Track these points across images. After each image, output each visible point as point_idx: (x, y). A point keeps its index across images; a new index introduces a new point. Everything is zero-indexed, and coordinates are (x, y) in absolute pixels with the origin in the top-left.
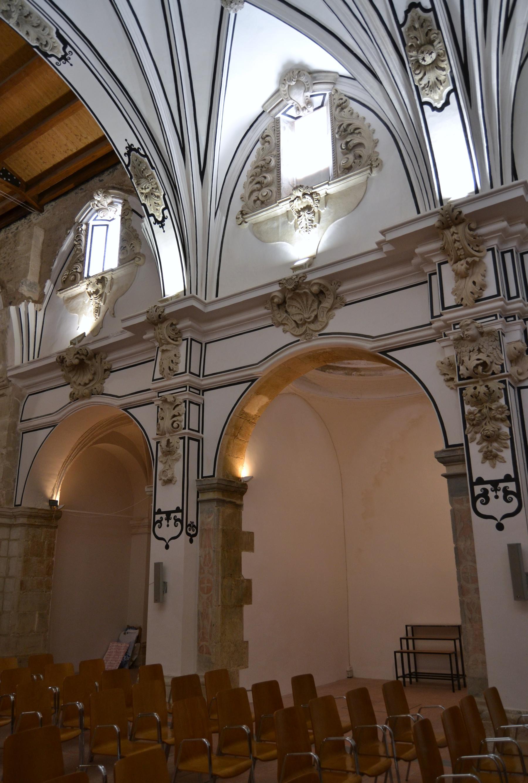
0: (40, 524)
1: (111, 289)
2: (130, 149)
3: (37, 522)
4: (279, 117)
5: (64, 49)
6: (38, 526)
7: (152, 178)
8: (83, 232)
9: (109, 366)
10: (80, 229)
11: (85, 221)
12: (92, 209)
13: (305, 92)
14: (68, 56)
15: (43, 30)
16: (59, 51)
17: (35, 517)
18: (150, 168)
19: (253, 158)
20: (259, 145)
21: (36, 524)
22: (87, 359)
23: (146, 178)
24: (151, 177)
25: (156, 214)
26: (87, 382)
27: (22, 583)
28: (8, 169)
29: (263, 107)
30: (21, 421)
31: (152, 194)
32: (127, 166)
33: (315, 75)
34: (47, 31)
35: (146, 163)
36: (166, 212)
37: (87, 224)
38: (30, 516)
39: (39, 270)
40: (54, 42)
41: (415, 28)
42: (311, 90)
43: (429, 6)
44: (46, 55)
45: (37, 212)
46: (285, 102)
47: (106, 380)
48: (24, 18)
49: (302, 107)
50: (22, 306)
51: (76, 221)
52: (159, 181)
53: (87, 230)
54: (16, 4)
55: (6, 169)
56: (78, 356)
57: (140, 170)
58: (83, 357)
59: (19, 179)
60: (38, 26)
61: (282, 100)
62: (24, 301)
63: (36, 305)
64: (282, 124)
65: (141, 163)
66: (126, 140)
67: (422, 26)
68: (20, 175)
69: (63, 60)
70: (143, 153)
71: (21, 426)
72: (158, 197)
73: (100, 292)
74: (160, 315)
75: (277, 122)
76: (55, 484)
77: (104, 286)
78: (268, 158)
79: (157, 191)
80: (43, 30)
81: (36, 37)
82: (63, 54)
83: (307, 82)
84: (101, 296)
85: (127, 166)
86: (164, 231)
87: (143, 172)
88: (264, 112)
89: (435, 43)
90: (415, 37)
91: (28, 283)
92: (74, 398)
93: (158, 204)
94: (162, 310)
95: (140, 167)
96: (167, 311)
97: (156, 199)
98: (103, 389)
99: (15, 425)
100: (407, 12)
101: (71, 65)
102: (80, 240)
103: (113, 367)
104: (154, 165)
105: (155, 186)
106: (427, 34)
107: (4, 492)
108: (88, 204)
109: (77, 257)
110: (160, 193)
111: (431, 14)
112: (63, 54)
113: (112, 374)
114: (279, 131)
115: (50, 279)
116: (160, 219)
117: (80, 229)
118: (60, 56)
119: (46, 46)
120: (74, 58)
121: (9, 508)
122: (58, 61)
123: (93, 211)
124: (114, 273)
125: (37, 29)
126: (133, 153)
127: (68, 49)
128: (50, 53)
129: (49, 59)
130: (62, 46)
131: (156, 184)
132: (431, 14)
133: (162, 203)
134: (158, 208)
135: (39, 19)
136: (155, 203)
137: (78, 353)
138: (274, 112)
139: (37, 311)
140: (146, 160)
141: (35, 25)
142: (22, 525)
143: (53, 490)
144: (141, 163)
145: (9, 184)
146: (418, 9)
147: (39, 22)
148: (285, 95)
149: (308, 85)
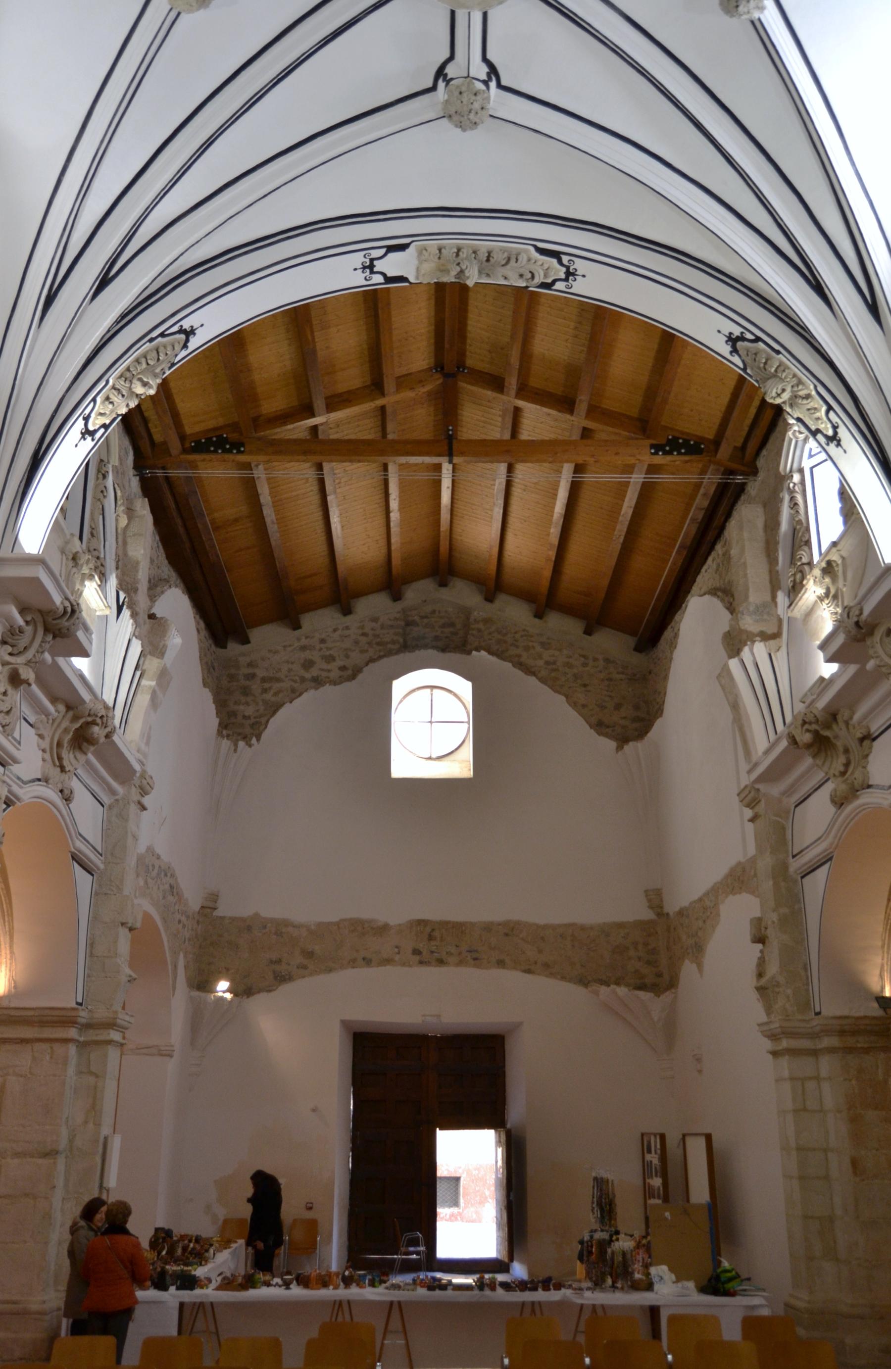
0: (866, 1046)
1: (845, 580)
2: (733, 340)
3: (862, 1042)
5: (560, 262)
6: (867, 1051)
7: (784, 371)
8: (796, 488)
9: (864, 731)
10: (791, 485)
11: (795, 466)
12: (797, 442)
14: (571, 268)
15: (516, 262)
16: (558, 271)
17: (854, 1033)
18: (774, 354)
21: (859, 1045)
22: (822, 729)
23: (775, 375)
24: (782, 368)
25: (821, 426)
26: (842, 769)
27: (854, 1163)
28: (677, 435)
30: (794, 857)
31: (796, 397)
32: (744, 370)
34: (523, 258)
35: (764, 350)
36: (832, 415)
37: (801, 471)
38: (842, 1033)
39: (767, 578)
40: (542, 265)
45: (751, 478)
47: (870, 758)
48: (487, 264)
50: (746, 653)
51: (783, 473)
52: (796, 370)
53: (803, 482)
54: (465, 256)
55: (674, 437)
56: (807, 726)
57: (759, 368)
58: (814, 727)
59: (700, 440)
62: (746, 644)
63: (767, 643)
66: (719, 331)
68: (698, 433)
69: (571, 278)
71: (795, 866)
72: (808, 397)
73: (833, 591)
74: (857, 623)
76: (882, 966)
77: (834, 580)
79: (800, 387)
80: (516, 262)
81: (517, 276)
82: (564, 269)
84: (835, 597)
85: (744, 370)
86: (845, 452)
87: (765, 369)
91: (752, 608)
92: (839, 802)
93: (815, 409)
94: (857, 612)
95: (757, 364)
96: (868, 609)
97: (805, 402)
98: (866, 776)
99: (785, 866)
101: (584, 276)
102: (796, 504)
103: (872, 730)
104: (777, 347)
105: (795, 381)
107: (789, 991)
108: (787, 439)
109: (800, 537)
110: (807, 388)
113: (876, 743)
115: (780, 588)
116: (830, 433)
117: (791, 485)
118: (563, 276)
119: (533, 277)
120: (580, 266)
121: (804, 1020)
122: (566, 283)
123: (800, 444)
124: (839, 547)
125: (508, 267)
126: (739, 344)
127: (565, 259)
128: (549, 281)
129: (554, 288)
131: (795, 376)
133: (818, 404)
134: (818, 415)
135: (504, 250)
136: (809, 410)
137: (804, 723)
139: (770, 655)
140: (761, 345)
141: (504, 262)
142: (831, 1050)
143: (881, 977)
144: (756, 354)
145: (687, 458)
147: (506, 255)
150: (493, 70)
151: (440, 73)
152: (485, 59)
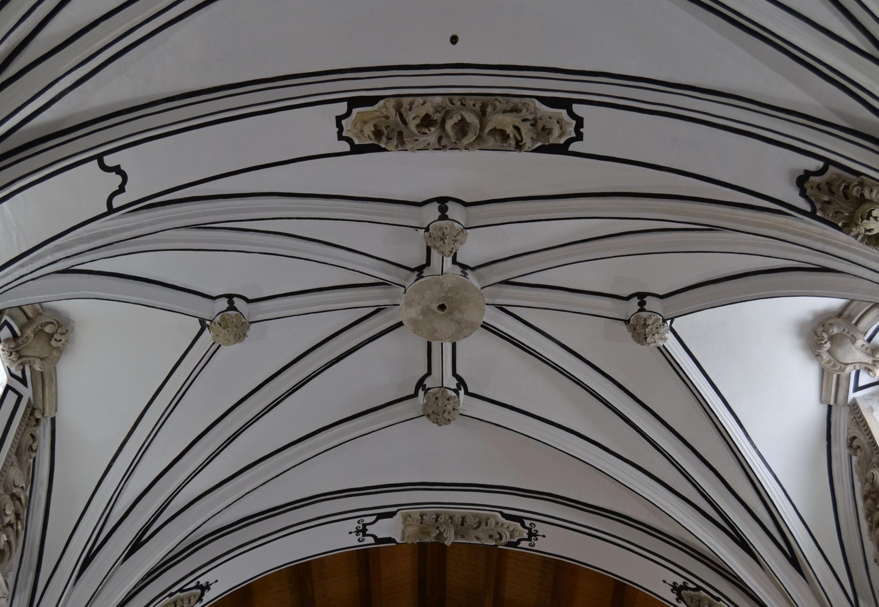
4: (854, 399)
5: (523, 525)
13: (853, 342)
15: (486, 525)
18: (715, 601)
19: (858, 485)
20: (854, 459)
29: (821, 401)
33: (846, 313)
34: (492, 522)
35: (705, 598)
41: (829, 203)
42: (858, 335)
43: (821, 164)
44: (515, 544)
46: (843, 375)
49: (870, 362)
60: (480, 524)
61: (838, 376)
64: (863, 407)
65: (699, 601)
66: (664, 582)
67: (832, 193)
70: (694, 587)
75: (854, 407)
78: (869, 475)
80: (486, 525)
82: (527, 531)
83: (844, 330)
88: (830, 408)
89: (867, 196)
90: (836, 213)
100: (803, 194)
101: (544, 536)
106: (846, 196)
111: (832, 169)
112: (527, 531)
114: (864, 419)
118: (526, 536)
120: (540, 528)
125: (480, 529)
127: (527, 523)
130: (518, 524)
132: (832, 169)
135: (475, 516)
138: (841, 398)
140: (703, 593)
141: (476, 526)
144: (699, 601)
146: (812, 178)
147: (477, 520)
148: (834, 366)
149: (848, 332)
150: (461, 382)
151: (420, 384)
152: (454, 374)
